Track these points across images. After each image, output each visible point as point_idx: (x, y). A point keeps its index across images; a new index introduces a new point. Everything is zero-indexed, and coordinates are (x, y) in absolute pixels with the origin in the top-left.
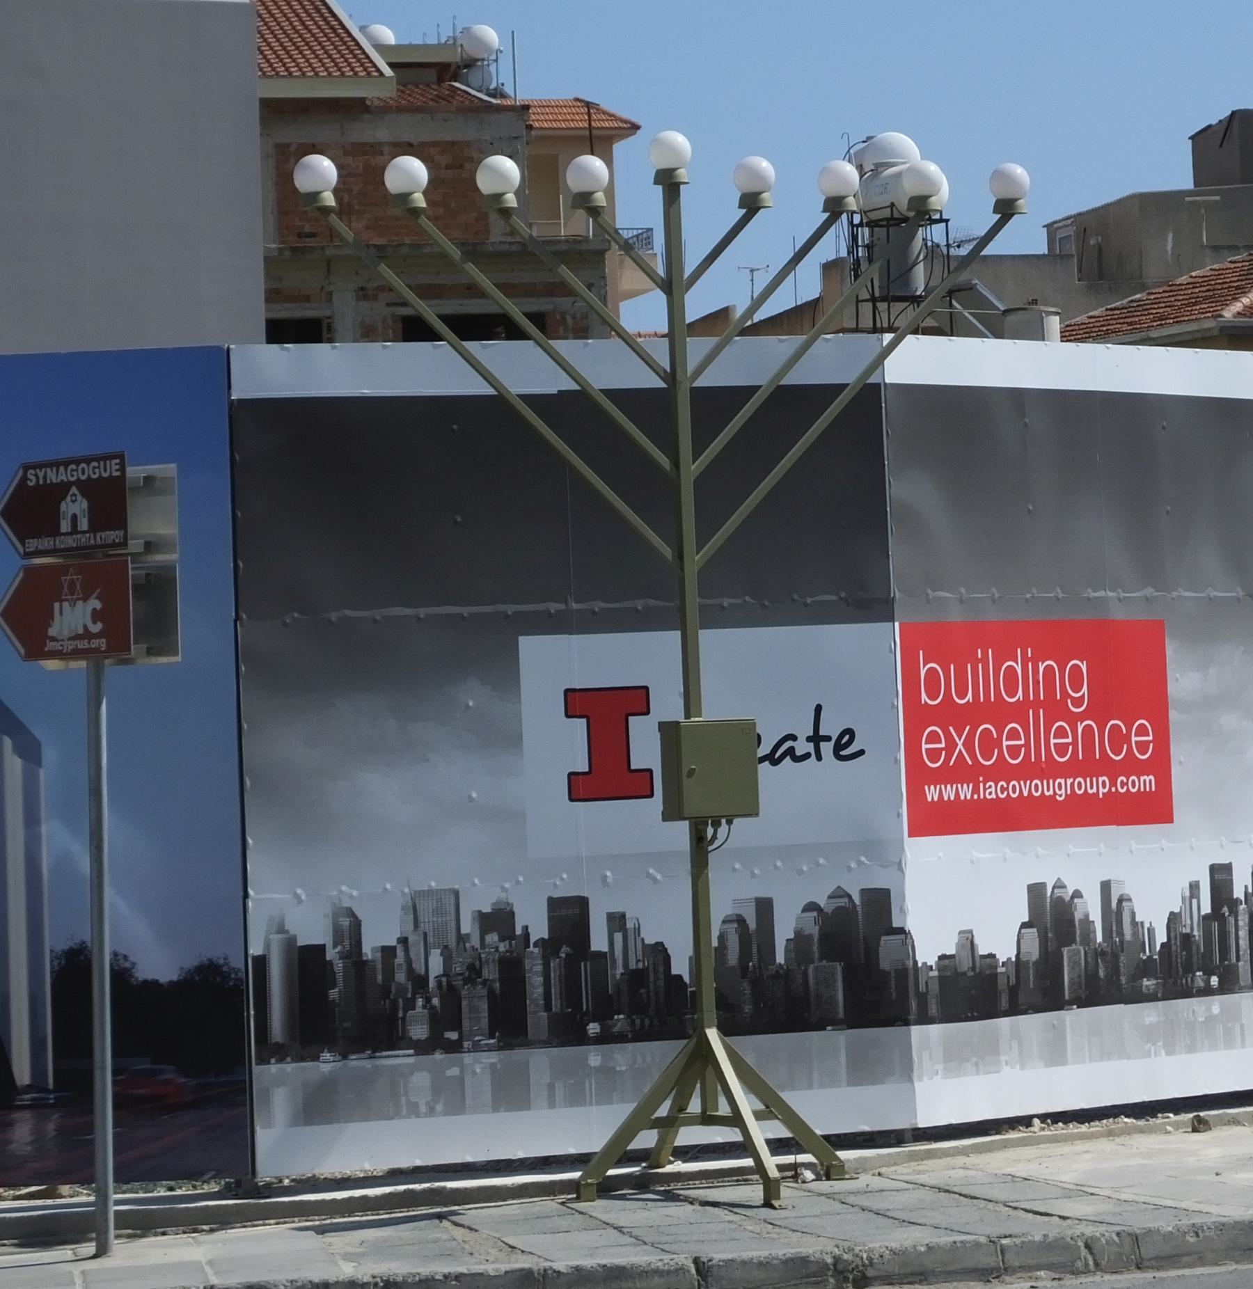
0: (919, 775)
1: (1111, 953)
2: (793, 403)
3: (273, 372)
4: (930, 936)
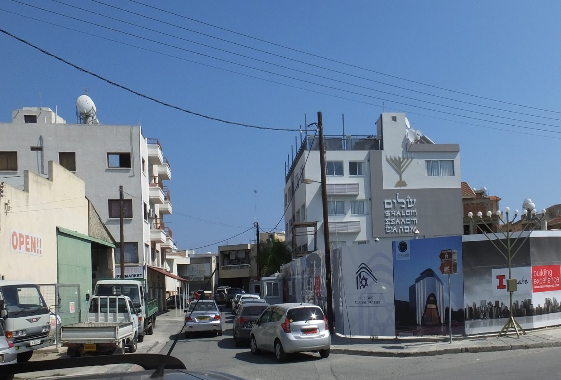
0: (534, 285)
1: (554, 307)
2: (521, 240)
3: (467, 238)
4: (535, 306)
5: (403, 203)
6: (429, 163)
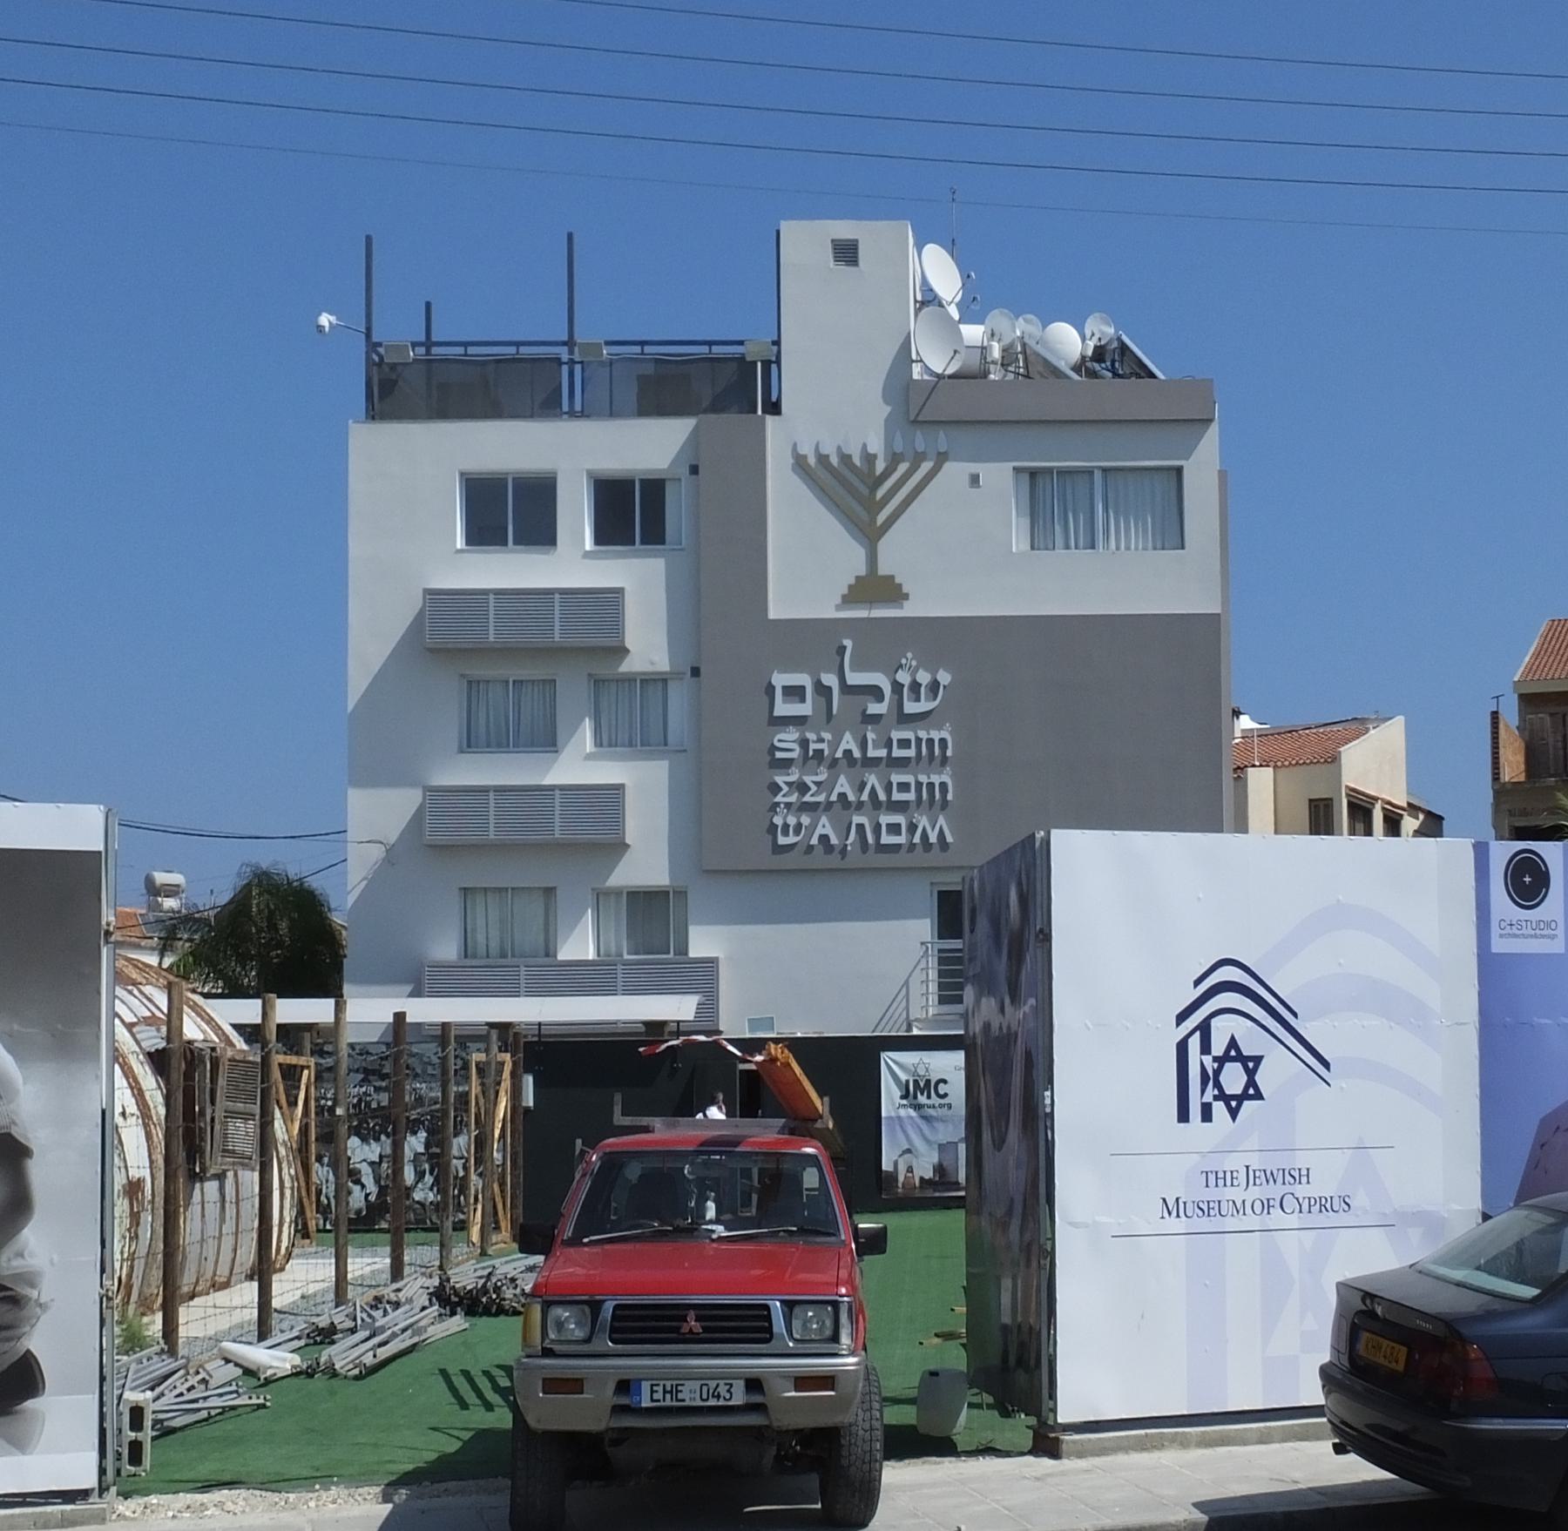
5: (875, 692)
6: (1040, 480)
